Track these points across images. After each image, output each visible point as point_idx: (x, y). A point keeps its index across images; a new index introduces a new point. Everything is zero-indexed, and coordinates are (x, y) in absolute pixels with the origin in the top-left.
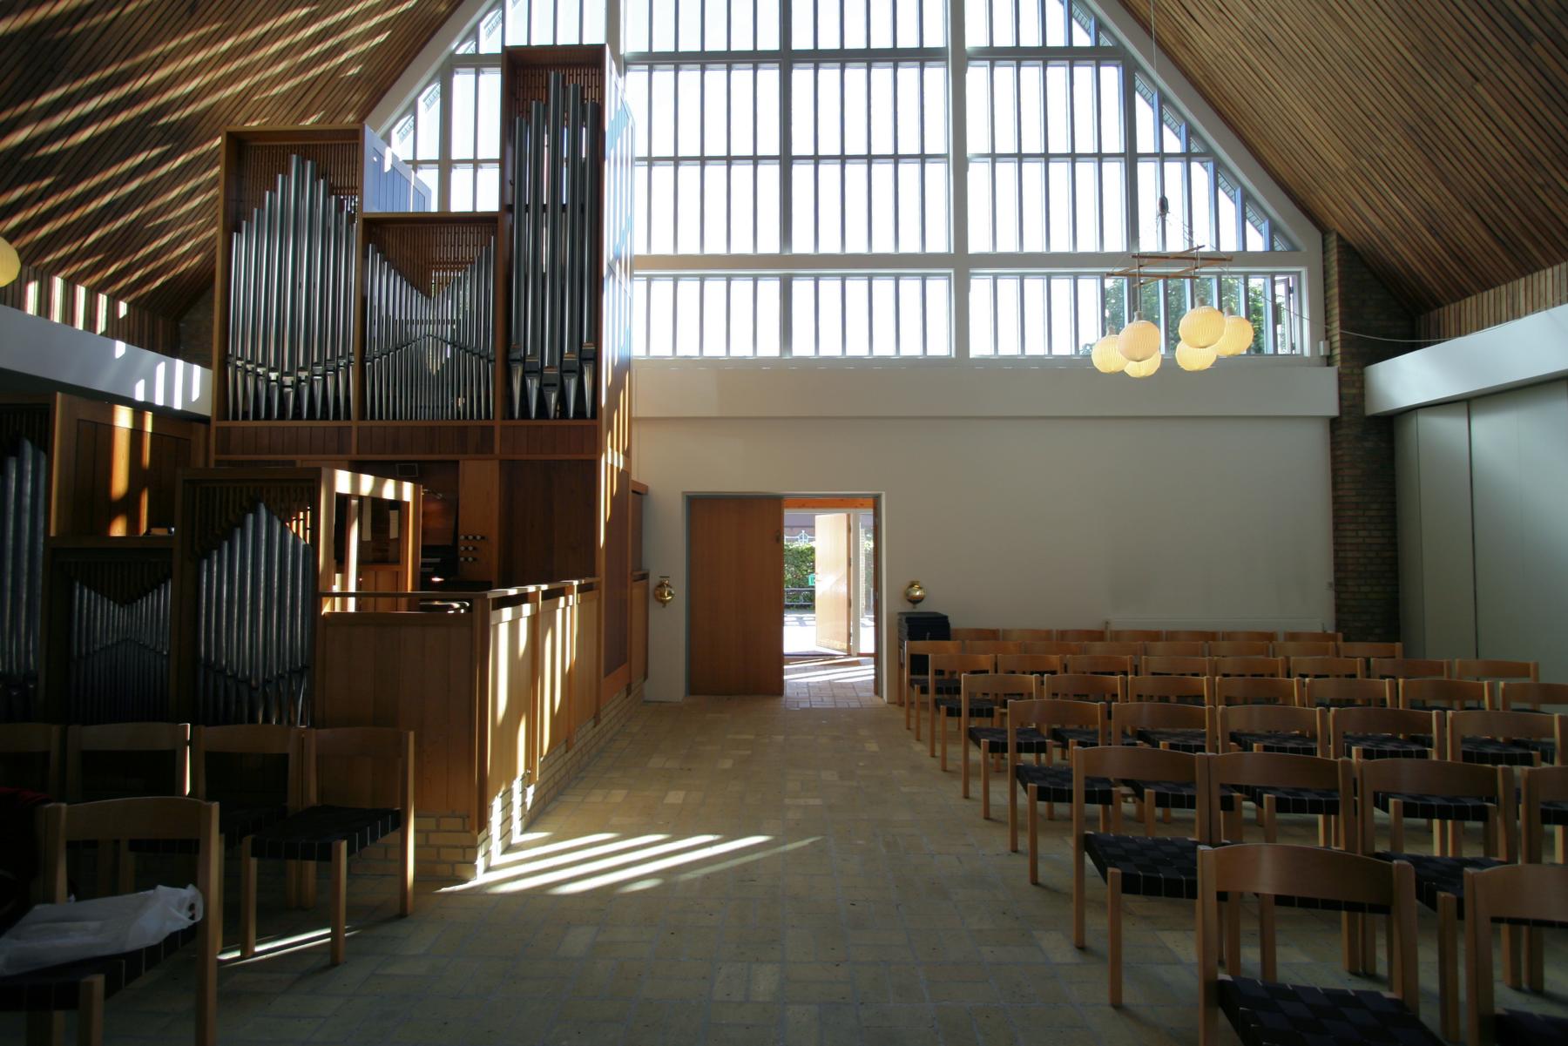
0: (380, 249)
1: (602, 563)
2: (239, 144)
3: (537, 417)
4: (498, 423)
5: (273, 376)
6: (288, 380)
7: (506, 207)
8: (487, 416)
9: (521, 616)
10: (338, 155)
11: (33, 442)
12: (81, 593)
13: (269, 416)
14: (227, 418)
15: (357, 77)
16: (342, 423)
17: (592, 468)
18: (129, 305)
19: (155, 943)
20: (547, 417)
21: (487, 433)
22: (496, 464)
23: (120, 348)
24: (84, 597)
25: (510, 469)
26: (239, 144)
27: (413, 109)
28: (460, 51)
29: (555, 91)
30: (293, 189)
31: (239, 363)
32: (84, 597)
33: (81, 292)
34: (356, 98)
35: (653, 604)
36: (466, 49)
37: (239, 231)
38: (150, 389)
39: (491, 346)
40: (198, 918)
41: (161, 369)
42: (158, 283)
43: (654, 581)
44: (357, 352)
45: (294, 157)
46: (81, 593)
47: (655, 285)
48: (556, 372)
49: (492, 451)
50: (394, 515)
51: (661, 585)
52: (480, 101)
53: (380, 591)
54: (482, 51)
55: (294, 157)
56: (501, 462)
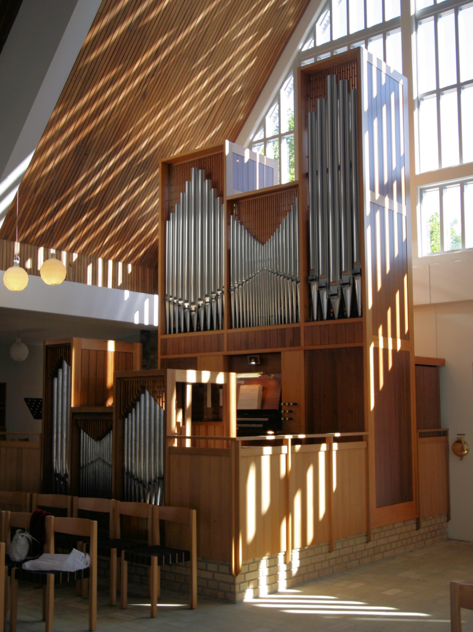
0: (239, 217)
1: (370, 422)
2: (168, 167)
3: (339, 318)
4: (302, 324)
5: (187, 305)
6: (193, 307)
7: (303, 175)
8: (297, 321)
9: (280, 453)
10: (211, 164)
11: (66, 361)
12: (83, 434)
13: (185, 331)
14: (166, 333)
15: (241, 92)
16: (220, 332)
17: (359, 355)
18: (133, 266)
19: (72, 571)
20: (345, 317)
21: (296, 331)
22: (302, 352)
23: (127, 293)
24: (84, 436)
25: (311, 357)
26: (168, 167)
27: (278, 98)
28: (305, 49)
29: (331, 85)
30: (195, 185)
31: (171, 299)
32: (84, 436)
33: (110, 263)
34: (242, 104)
35: (453, 459)
36: (309, 45)
37: (169, 219)
38: (142, 316)
39: (299, 273)
40: (88, 566)
41: (147, 303)
42: (142, 253)
43: (452, 438)
44: (226, 287)
45: (193, 169)
46: (83, 434)
47: (446, 193)
48: (338, 287)
49: (299, 345)
50: (221, 391)
51: (459, 441)
52: (282, 108)
53: (216, 436)
54: (318, 44)
55: (193, 169)
56: (305, 351)
